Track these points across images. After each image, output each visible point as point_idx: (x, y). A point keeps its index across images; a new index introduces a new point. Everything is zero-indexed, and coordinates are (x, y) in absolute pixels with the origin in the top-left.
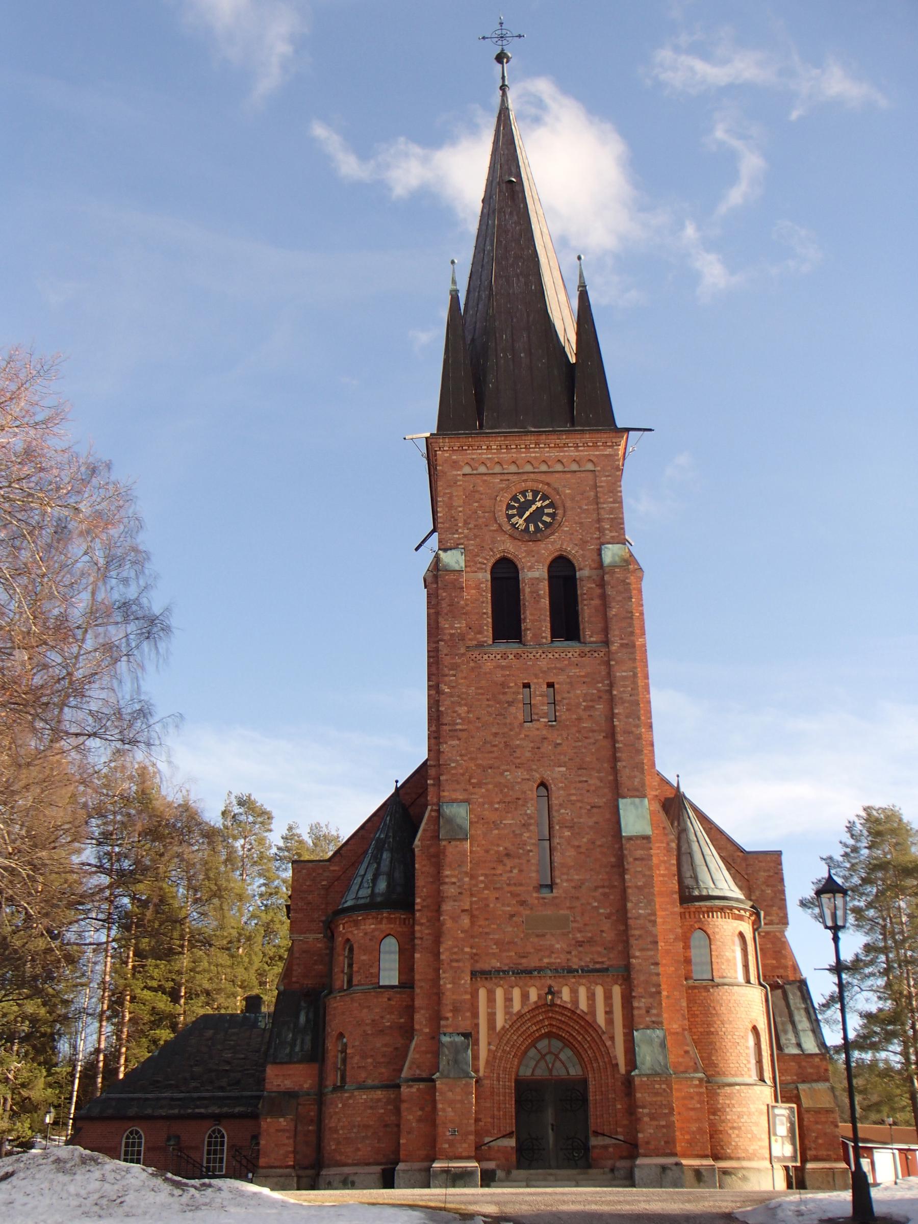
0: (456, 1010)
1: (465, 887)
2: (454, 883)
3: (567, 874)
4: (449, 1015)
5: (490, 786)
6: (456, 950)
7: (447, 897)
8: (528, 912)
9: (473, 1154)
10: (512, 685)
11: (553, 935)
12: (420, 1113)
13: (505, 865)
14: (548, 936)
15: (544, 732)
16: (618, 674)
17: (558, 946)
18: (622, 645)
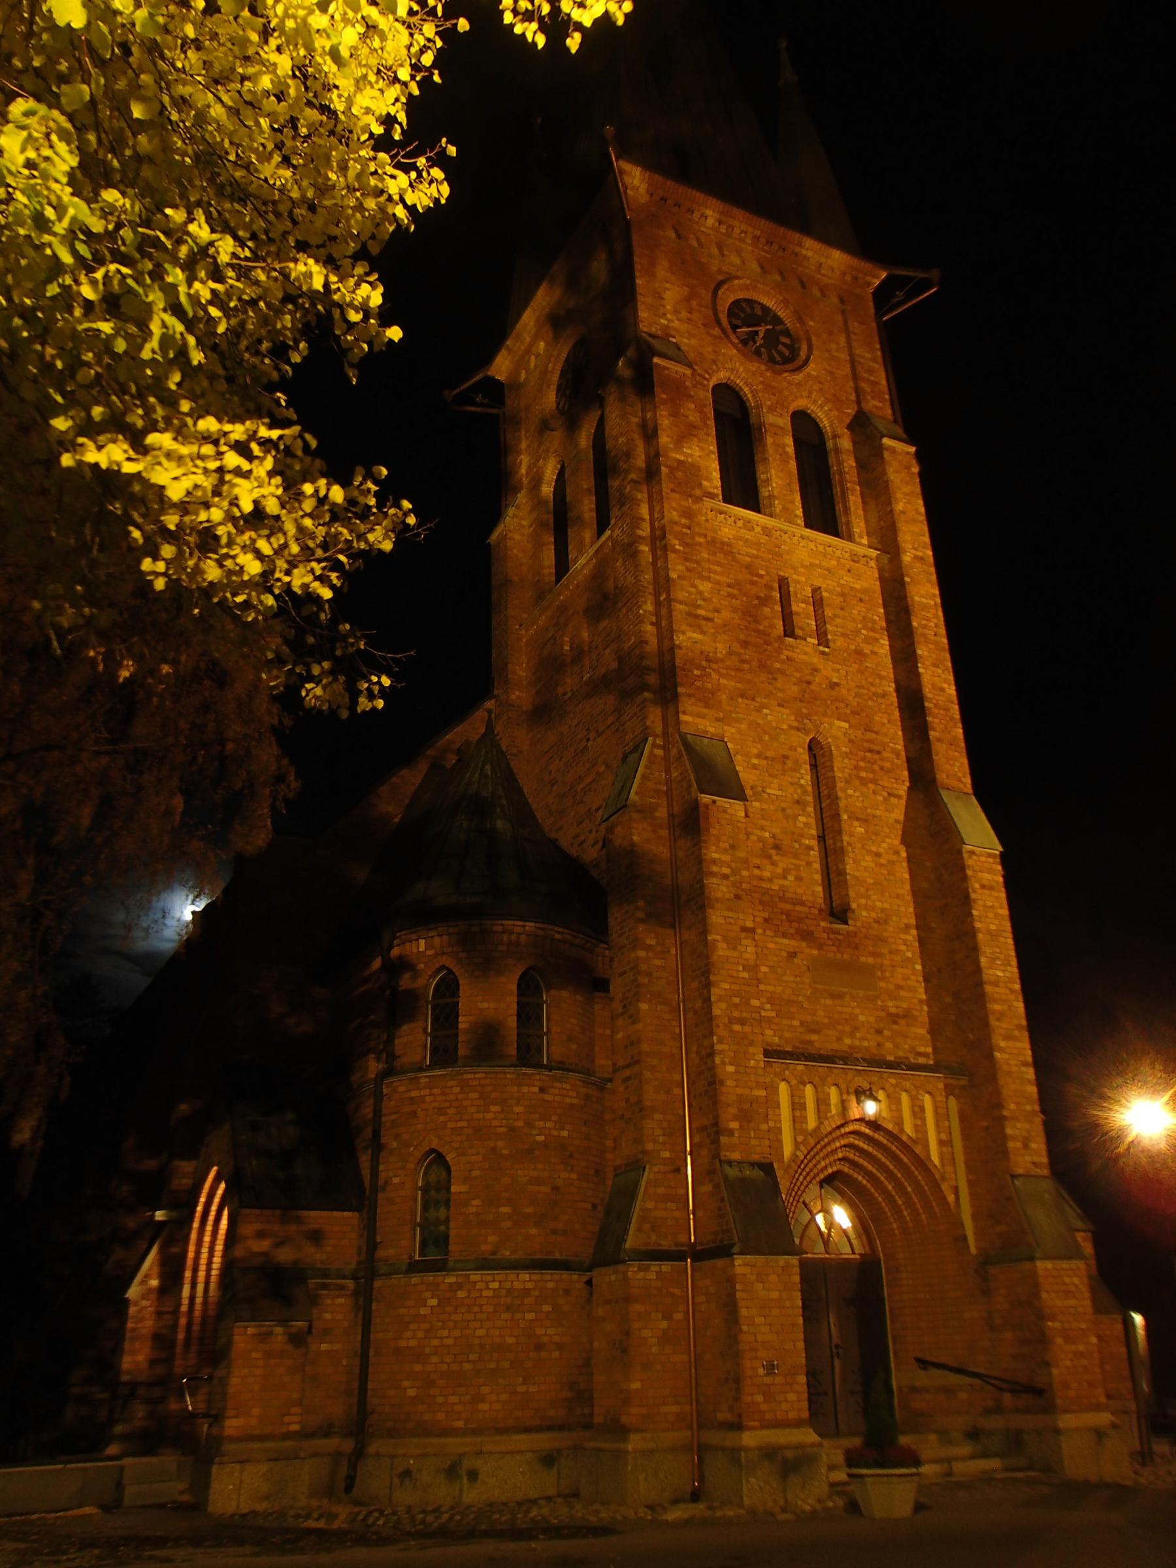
0: (745, 1116)
1: (744, 886)
2: (725, 877)
3: (868, 897)
4: (734, 1125)
5: (744, 726)
6: (737, 1000)
7: (717, 900)
8: (815, 952)
9: (805, 1414)
10: (763, 572)
11: (853, 998)
12: (664, 1324)
13: (774, 864)
14: (847, 998)
15: (815, 660)
16: (917, 599)
17: (862, 1018)
18: (916, 557)
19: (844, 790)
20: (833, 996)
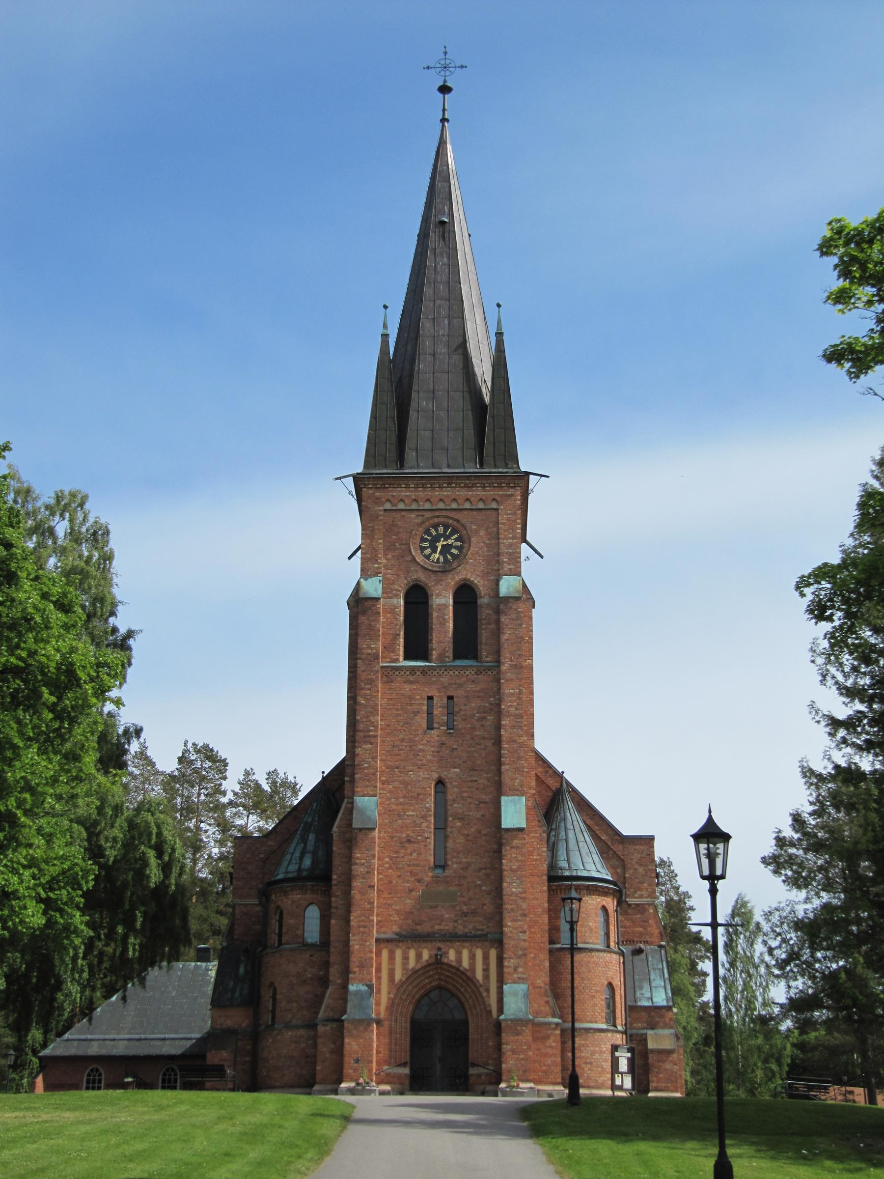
2: (363, 864)
4: (356, 969)
12: (332, 1046)
19: (452, 805)
20: (431, 907)
